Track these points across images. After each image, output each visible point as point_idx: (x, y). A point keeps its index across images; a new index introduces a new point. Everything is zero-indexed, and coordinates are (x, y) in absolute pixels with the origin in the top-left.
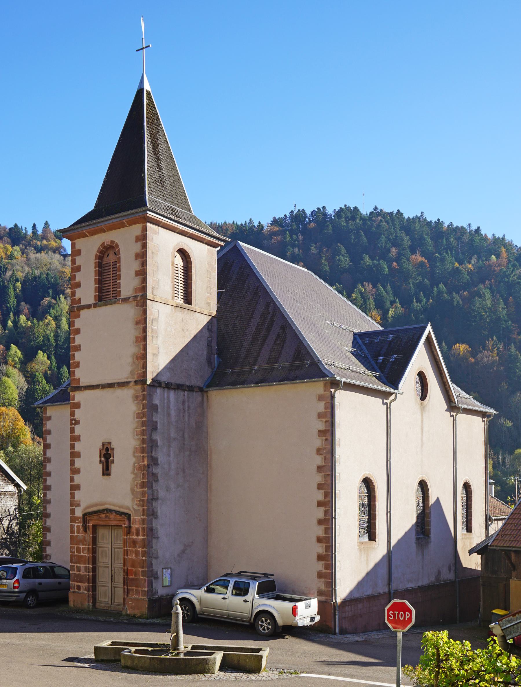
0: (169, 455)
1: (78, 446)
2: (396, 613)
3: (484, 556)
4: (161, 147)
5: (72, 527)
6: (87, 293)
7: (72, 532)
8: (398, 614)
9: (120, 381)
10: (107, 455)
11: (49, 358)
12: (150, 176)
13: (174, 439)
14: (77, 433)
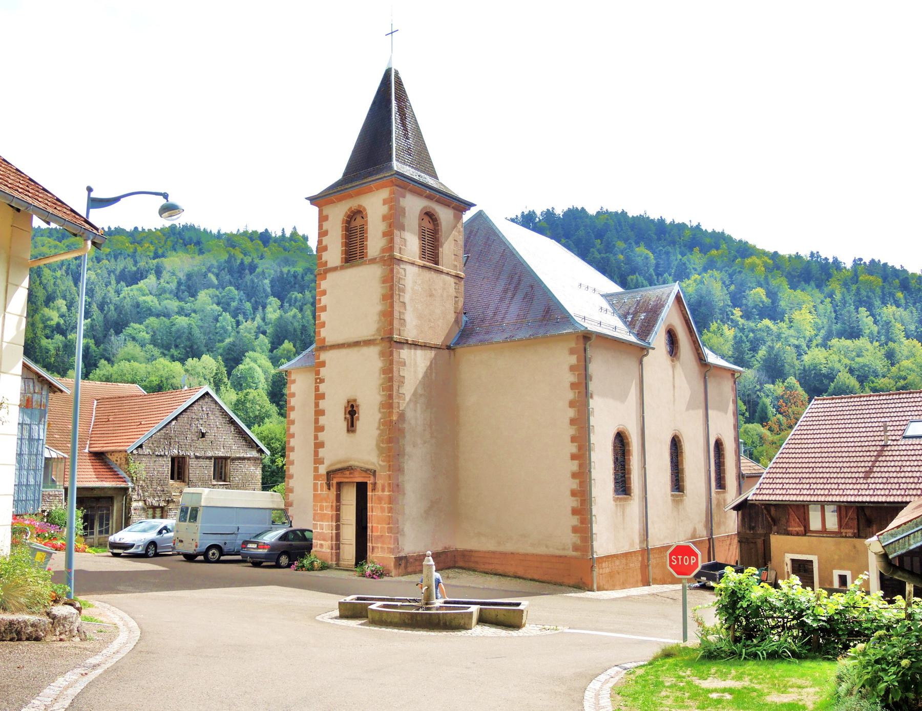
0: (415, 411)
1: (323, 404)
2: (680, 557)
3: (740, 512)
4: (408, 112)
5: (315, 485)
6: (334, 256)
7: (315, 489)
8: (682, 559)
9: (366, 338)
10: (352, 412)
11: (294, 346)
12: (397, 143)
13: (421, 395)
14: (321, 391)
